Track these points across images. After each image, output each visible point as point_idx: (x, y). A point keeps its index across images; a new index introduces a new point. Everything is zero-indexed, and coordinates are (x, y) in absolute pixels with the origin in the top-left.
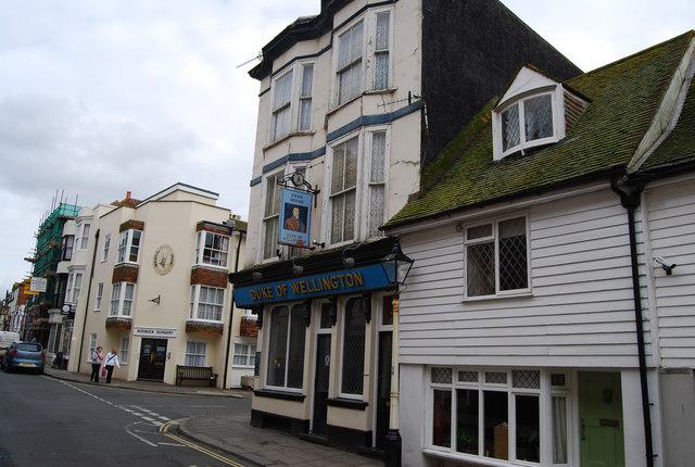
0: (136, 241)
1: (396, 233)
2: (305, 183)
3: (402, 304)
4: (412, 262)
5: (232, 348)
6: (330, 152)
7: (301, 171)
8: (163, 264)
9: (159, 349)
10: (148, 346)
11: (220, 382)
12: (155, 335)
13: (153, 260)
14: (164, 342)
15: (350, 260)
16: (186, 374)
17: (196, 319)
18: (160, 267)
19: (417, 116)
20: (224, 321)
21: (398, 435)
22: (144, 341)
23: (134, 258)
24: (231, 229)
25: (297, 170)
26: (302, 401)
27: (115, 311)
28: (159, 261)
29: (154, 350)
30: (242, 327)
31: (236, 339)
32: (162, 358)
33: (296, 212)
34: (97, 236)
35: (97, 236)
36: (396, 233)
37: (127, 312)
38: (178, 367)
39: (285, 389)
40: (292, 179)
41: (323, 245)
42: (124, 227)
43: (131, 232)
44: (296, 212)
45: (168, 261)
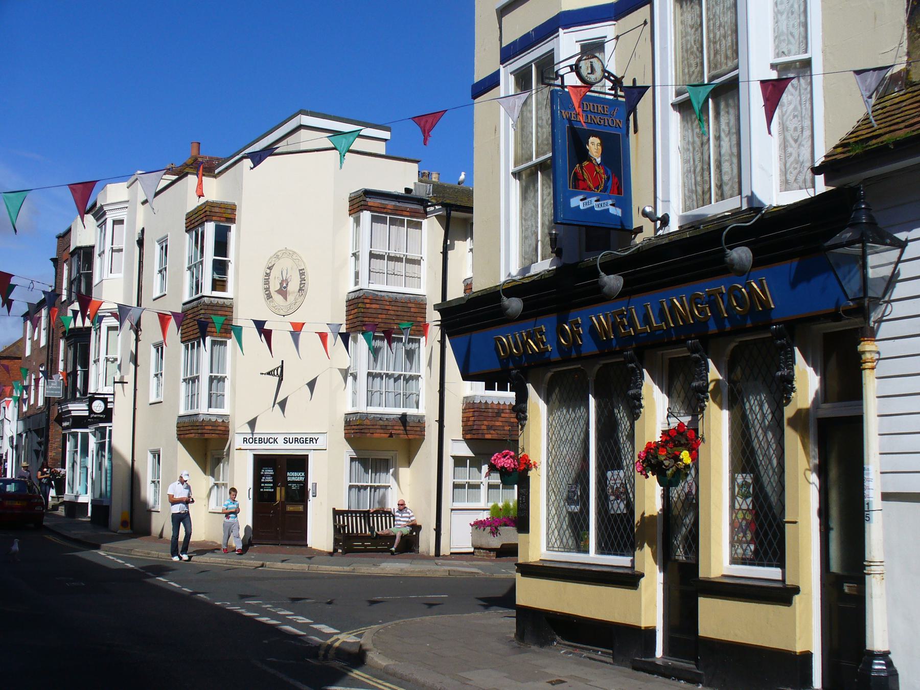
0: (221, 247)
1: (853, 179)
2: (607, 75)
3: (886, 348)
4: (902, 245)
5: (448, 464)
6: (508, 84)
7: (592, 49)
8: (283, 292)
9: (294, 476)
10: (270, 472)
11: (427, 541)
12: (281, 448)
13: (260, 286)
14: (300, 463)
15: (741, 254)
16: (357, 526)
17: (363, 408)
18: (278, 298)
19: (555, 63)
20: (426, 409)
21: (889, 664)
22: (261, 462)
23: (219, 284)
24: (423, 202)
25: (583, 47)
26: (123, 224)
27: (192, 398)
28: (275, 286)
29: (280, 478)
30: (465, 421)
31: (456, 447)
32: (301, 494)
33: (594, 146)
34: (141, 243)
35: (141, 243)
36: (853, 179)
37: (214, 399)
38: (336, 513)
39: (593, 557)
40: (576, 69)
41: (665, 220)
42: (194, 222)
43: (210, 229)
44: (594, 146)
45: (293, 286)
